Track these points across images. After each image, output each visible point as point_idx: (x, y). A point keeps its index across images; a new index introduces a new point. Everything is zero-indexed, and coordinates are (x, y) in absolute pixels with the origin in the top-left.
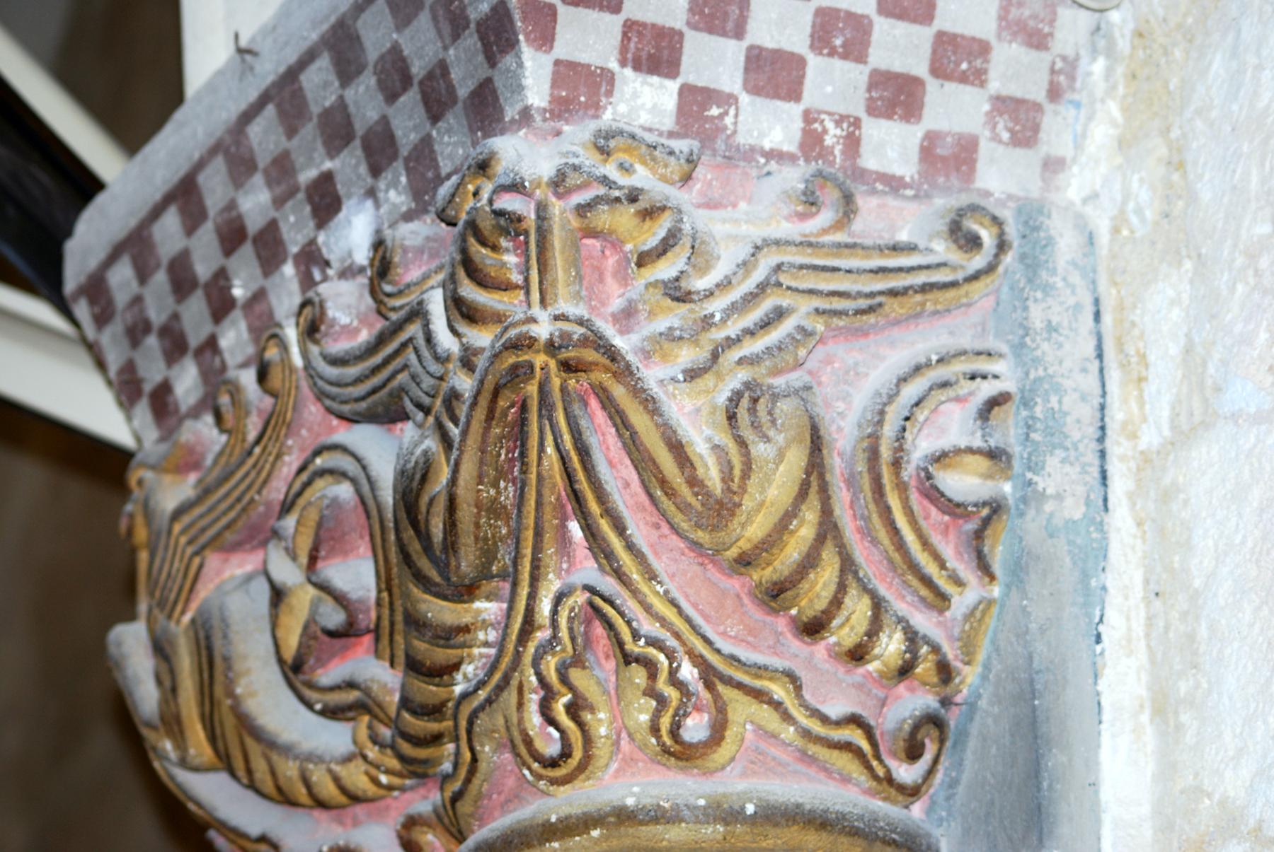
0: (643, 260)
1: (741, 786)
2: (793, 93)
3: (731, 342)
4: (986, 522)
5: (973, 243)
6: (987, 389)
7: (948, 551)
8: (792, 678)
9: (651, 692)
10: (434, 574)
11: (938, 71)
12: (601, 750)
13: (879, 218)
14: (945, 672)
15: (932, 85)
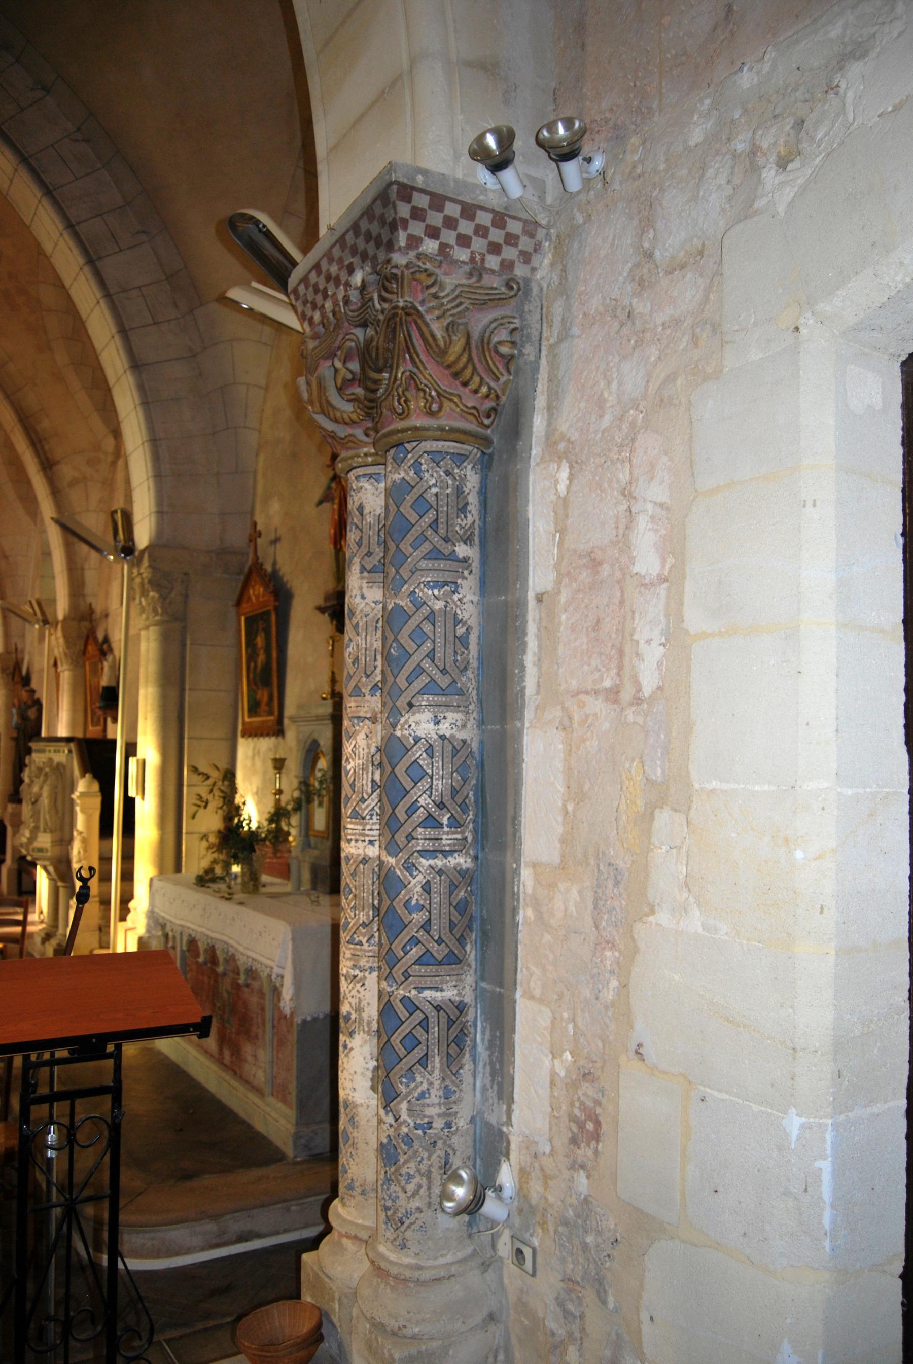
0: (428, 287)
1: (445, 423)
2: (468, 246)
3: (448, 310)
4: (510, 360)
5: (512, 288)
6: (512, 326)
7: (500, 367)
8: (459, 396)
9: (424, 398)
10: (371, 365)
11: (506, 243)
12: (412, 412)
13: (487, 280)
14: (497, 397)
15: (504, 246)
